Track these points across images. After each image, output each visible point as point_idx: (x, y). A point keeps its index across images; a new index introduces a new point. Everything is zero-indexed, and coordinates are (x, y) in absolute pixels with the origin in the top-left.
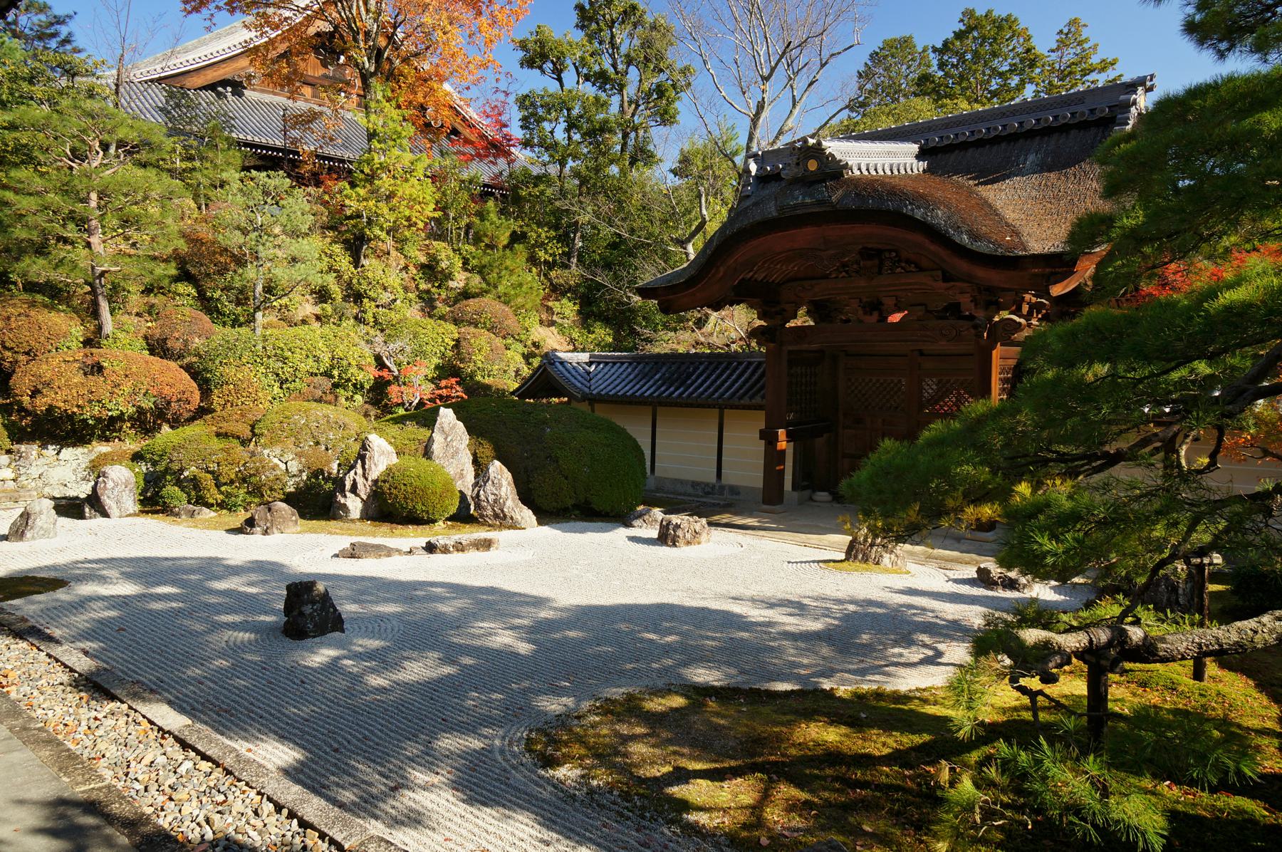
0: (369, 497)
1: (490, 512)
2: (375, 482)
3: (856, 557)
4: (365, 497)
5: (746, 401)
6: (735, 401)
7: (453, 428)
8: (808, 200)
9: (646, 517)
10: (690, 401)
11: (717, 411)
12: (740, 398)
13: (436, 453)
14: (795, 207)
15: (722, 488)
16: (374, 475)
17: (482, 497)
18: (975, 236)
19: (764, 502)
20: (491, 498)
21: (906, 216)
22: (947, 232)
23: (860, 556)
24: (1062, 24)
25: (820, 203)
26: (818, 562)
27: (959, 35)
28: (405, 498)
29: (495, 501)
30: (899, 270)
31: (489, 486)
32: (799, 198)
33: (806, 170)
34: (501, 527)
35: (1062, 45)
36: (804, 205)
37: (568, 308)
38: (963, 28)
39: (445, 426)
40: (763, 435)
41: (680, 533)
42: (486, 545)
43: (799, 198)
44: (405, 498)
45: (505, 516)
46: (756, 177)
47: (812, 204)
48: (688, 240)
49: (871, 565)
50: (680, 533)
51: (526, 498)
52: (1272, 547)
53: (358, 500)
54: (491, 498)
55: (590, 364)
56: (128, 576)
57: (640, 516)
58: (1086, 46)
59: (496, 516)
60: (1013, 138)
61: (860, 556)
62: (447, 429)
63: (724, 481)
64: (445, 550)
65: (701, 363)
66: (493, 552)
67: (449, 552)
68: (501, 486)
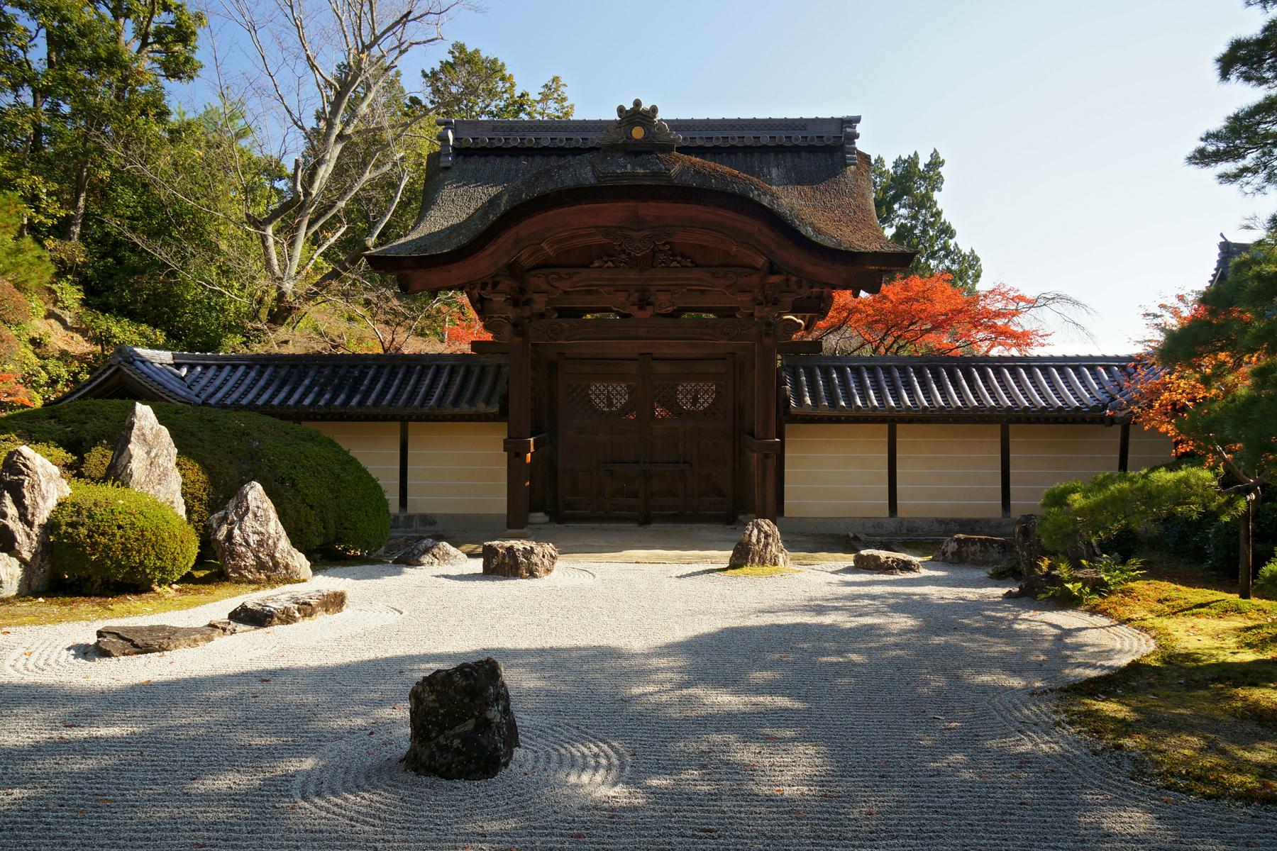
0: (35, 555)
1: (251, 561)
2: (51, 526)
3: (753, 561)
4: (27, 556)
5: (464, 408)
6: (449, 409)
7: (157, 436)
8: (640, 171)
9: (435, 551)
10: (426, 410)
11: (398, 424)
12: (455, 403)
13: (136, 476)
14: (619, 176)
15: (410, 518)
16: (42, 517)
17: (238, 539)
18: (818, 231)
19: (509, 526)
20: (253, 539)
21: (752, 201)
22: (793, 222)
23: (757, 559)
24: (547, 79)
25: (655, 175)
26: (690, 575)
27: (446, 66)
28: (126, 550)
29: (260, 543)
30: (674, 264)
31: (249, 521)
32: (626, 166)
33: (630, 137)
34: (270, 582)
35: (545, 98)
36: (633, 175)
37: (71, 295)
38: (451, 60)
39: (147, 432)
40: (507, 446)
41: (534, 559)
42: (335, 602)
43: (626, 166)
44: (126, 550)
45: (276, 565)
46: (453, 147)
47: (645, 175)
48: (268, 221)
49: (768, 569)
50: (534, 559)
51: (298, 541)
52: (1272, 476)
53: (15, 562)
54: (253, 539)
55: (178, 366)
56: (533, 668)
57: (427, 551)
58: (565, 104)
59: (261, 566)
60: (765, 149)
61: (757, 559)
62: (150, 438)
63: (411, 510)
64: (287, 618)
65: (369, 367)
66: (347, 611)
67: (295, 620)
68: (268, 520)
